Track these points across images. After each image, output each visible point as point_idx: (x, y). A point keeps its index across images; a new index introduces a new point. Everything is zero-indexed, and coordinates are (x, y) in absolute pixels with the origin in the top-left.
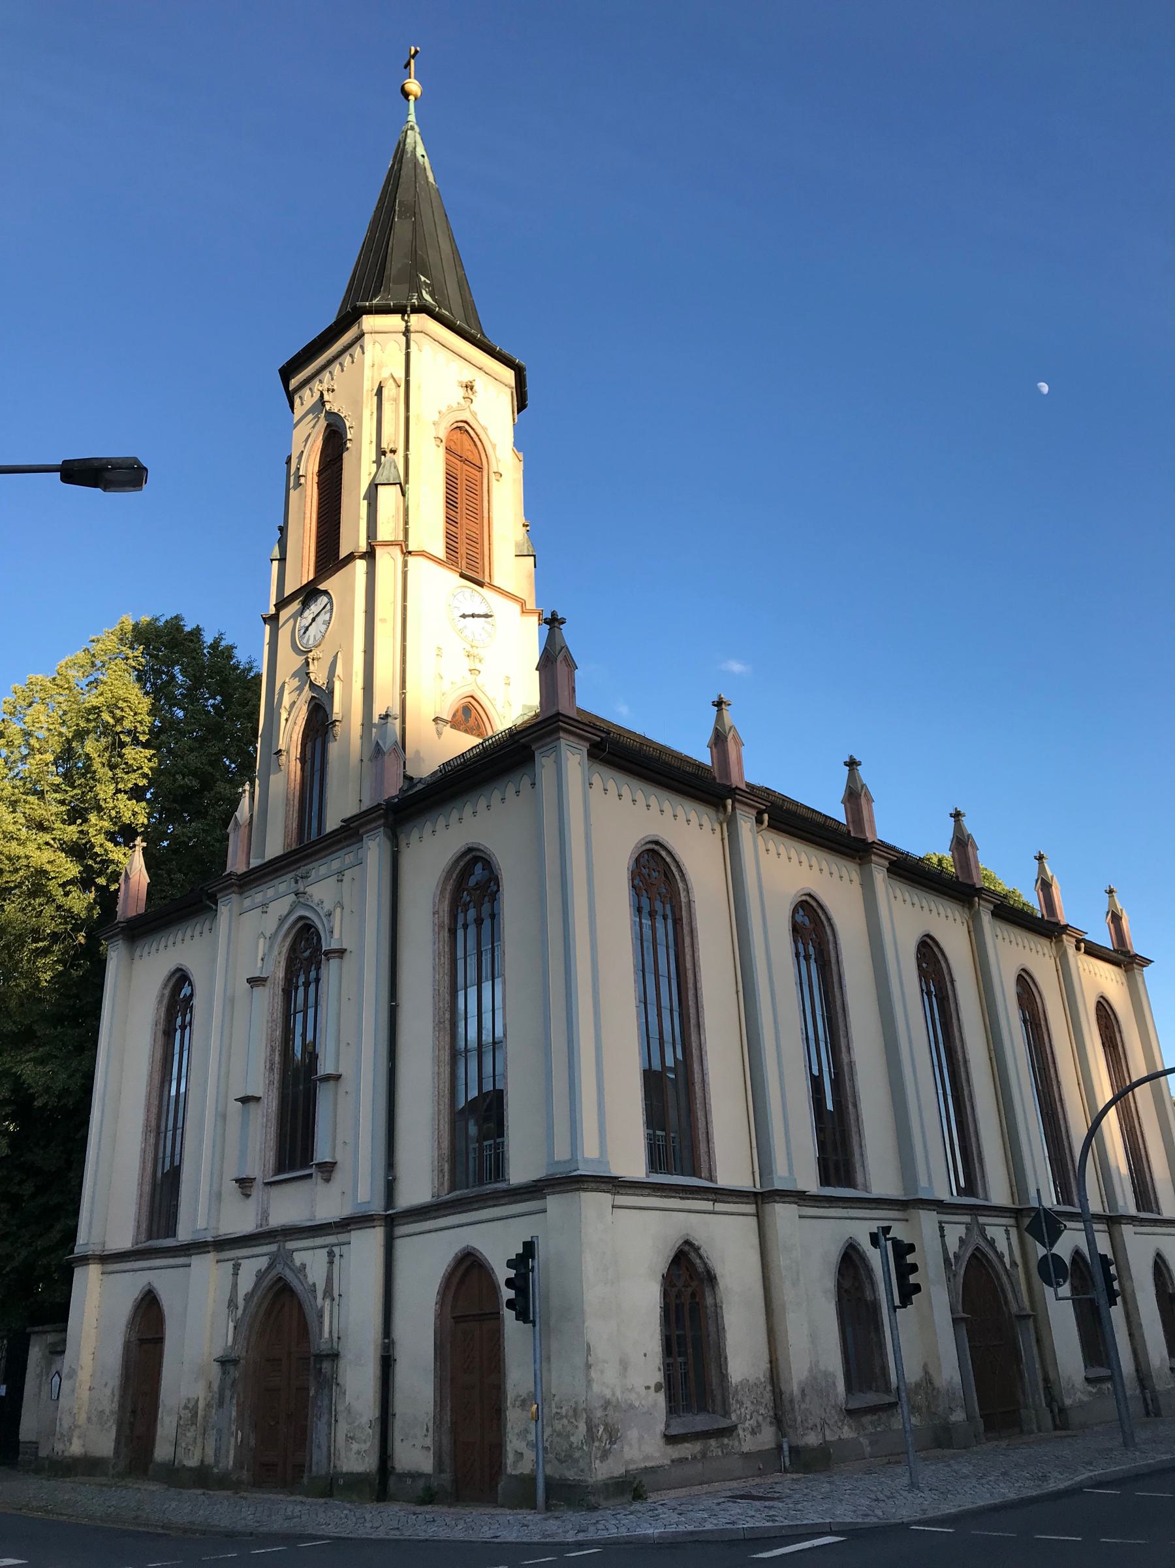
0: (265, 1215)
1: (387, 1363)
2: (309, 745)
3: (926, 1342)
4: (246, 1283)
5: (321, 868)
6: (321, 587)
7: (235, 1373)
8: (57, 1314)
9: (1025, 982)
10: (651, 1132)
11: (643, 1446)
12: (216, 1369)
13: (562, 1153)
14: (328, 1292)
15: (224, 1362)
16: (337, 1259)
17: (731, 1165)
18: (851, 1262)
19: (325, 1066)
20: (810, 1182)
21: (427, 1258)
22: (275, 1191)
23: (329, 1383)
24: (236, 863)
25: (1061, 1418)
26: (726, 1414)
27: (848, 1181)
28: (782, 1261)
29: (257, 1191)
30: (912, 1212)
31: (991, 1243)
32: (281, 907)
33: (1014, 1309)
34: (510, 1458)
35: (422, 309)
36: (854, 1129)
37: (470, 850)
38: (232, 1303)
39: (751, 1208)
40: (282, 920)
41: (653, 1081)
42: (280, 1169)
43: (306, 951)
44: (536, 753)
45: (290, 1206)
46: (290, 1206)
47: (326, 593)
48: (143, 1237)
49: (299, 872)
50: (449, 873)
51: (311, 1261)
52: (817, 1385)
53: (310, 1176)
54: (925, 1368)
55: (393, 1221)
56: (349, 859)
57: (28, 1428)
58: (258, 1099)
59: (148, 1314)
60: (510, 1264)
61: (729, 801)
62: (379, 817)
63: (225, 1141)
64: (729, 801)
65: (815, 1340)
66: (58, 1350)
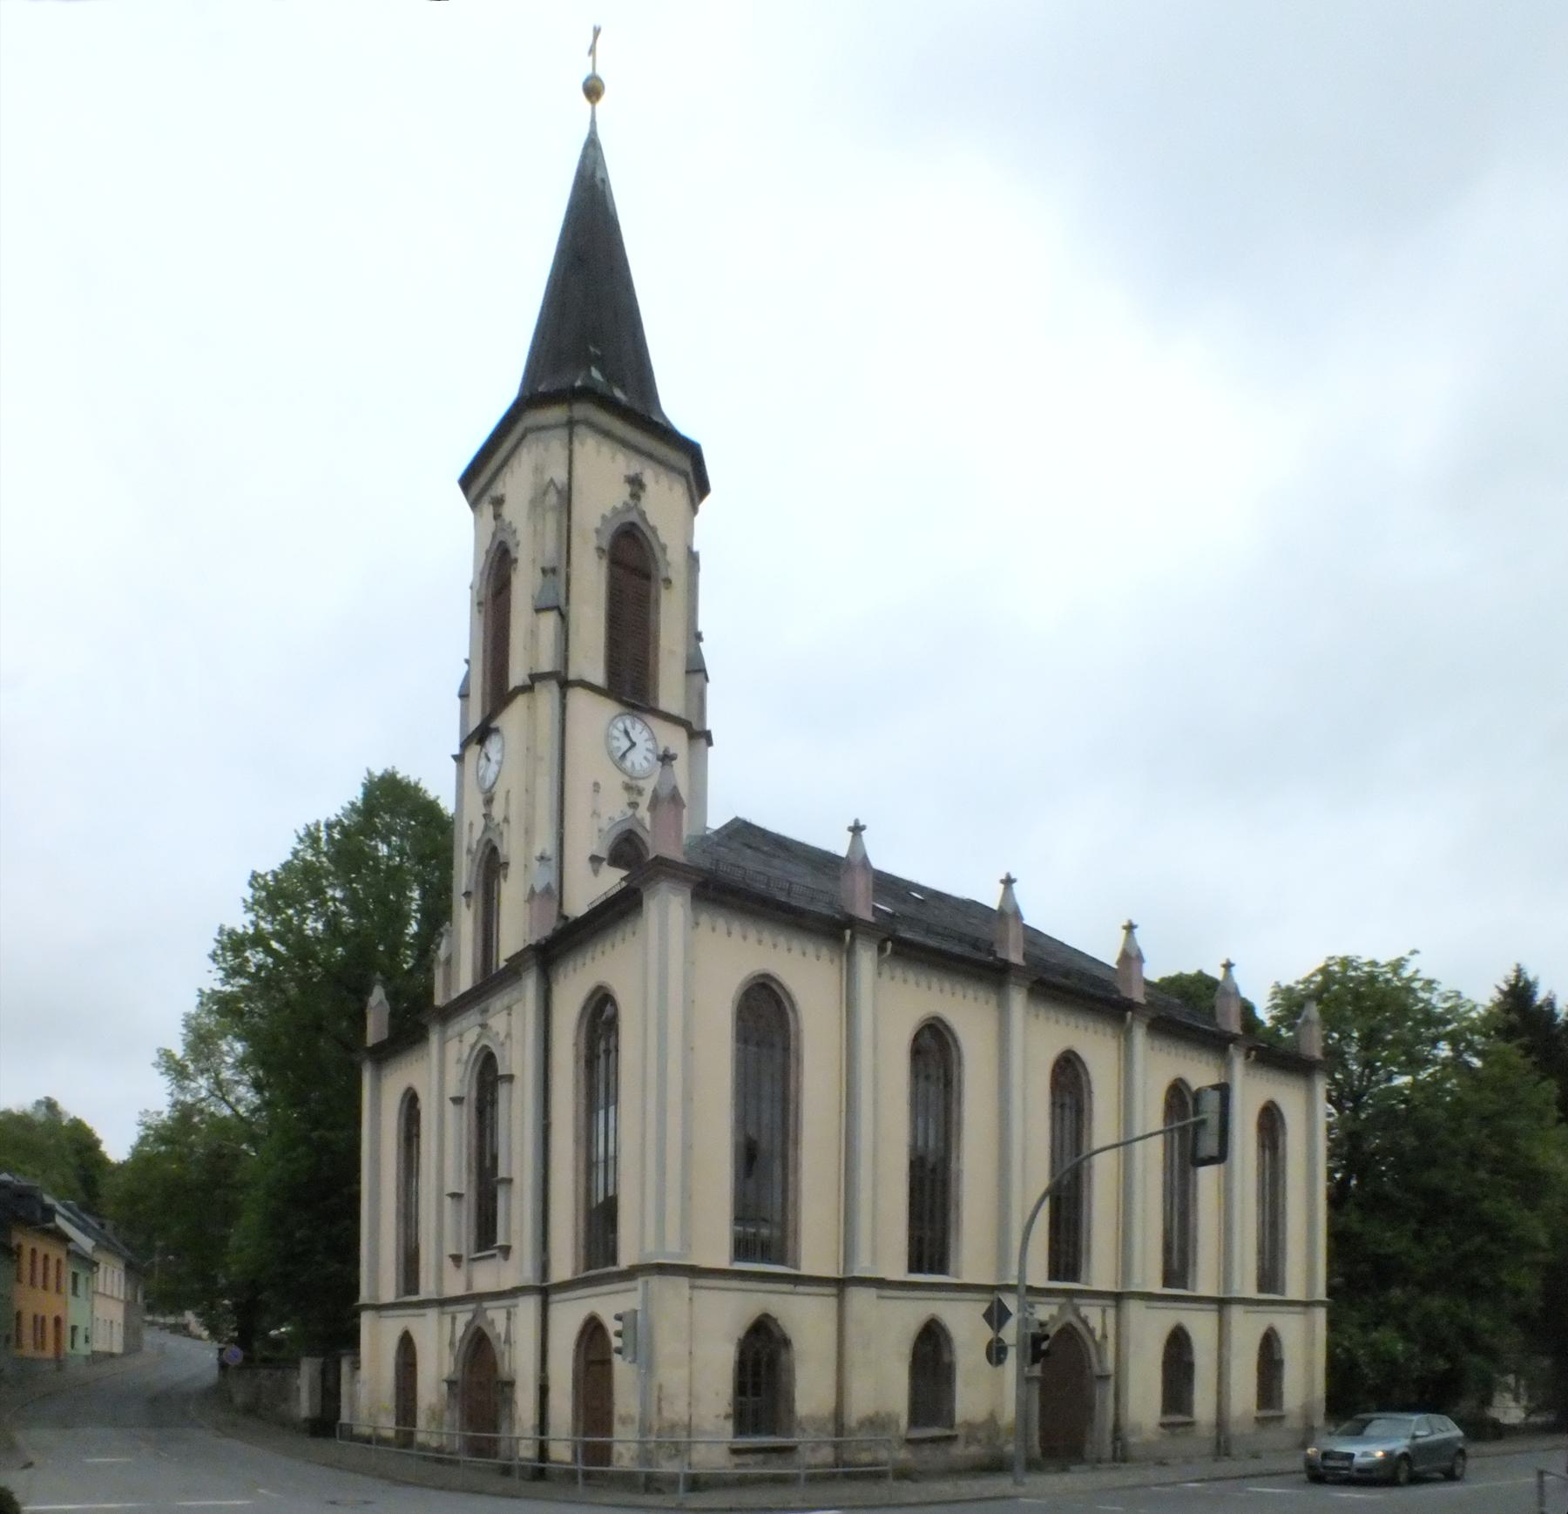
0: (469, 1285)
1: (543, 1391)
3: (987, 1392)
4: (460, 1330)
5: (498, 1002)
6: (493, 725)
8: (351, 1340)
10: (740, 1229)
11: (712, 1456)
12: (445, 1386)
13: (650, 1246)
14: (508, 1341)
17: (816, 1252)
19: (502, 1173)
21: (568, 1318)
23: (509, 1401)
24: (439, 1000)
25: (1121, 1454)
27: (940, 1266)
28: (851, 1329)
31: (1084, 1322)
32: (471, 1036)
33: (1097, 1370)
35: (588, 394)
38: (452, 1344)
39: (833, 1290)
40: (473, 1047)
41: (918, 1166)
43: (488, 1075)
45: (488, 1277)
46: (488, 1277)
48: (581, 1268)
49: (483, 1005)
50: (584, 1008)
51: (496, 1315)
52: (876, 1423)
53: (493, 1256)
55: (545, 1292)
56: (515, 994)
57: (345, 1418)
59: (406, 1344)
61: (848, 933)
63: (446, 1227)
64: (848, 933)
65: (884, 1386)
66: (356, 1366)
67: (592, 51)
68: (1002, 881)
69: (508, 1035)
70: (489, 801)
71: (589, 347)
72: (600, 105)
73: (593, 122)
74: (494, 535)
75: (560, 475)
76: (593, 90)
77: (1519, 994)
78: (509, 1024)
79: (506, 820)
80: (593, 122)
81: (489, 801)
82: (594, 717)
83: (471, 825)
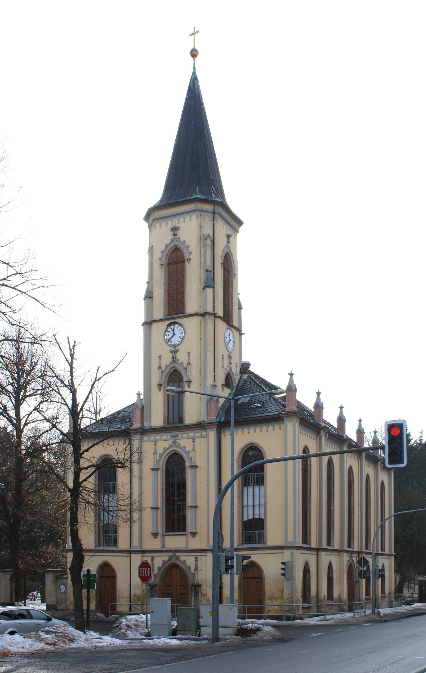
0: (163, 546)
2: (209, 403)
14: (196, 569)
16: (199, 560)
18: (350, 567)
22: (166, 538)
29: (159, 537)
30: (342, 553)
36: (332, 529)
37: (252, 444)
39: (315, 553)
40: (165, 450)
42: (168, 530)
44: (285, 420)
45: (175, 542)
47: (180, 325)
54: (339, 594)
60: (184, 561)
62: (215, 425)
67: (113, 370)
68: (316, 393)
69: (194, 450)
70: (174, 352)
71: (193, 171)
72: (196, 59)
73: (194, 68)
74: (172, 241)
75: (211, 234)
76: (194, 54)
77: (396, 432)
78: (194, 445)
79: (189, 364)
80: (194, 68)
81: (174, 352)
82: (221, 325)
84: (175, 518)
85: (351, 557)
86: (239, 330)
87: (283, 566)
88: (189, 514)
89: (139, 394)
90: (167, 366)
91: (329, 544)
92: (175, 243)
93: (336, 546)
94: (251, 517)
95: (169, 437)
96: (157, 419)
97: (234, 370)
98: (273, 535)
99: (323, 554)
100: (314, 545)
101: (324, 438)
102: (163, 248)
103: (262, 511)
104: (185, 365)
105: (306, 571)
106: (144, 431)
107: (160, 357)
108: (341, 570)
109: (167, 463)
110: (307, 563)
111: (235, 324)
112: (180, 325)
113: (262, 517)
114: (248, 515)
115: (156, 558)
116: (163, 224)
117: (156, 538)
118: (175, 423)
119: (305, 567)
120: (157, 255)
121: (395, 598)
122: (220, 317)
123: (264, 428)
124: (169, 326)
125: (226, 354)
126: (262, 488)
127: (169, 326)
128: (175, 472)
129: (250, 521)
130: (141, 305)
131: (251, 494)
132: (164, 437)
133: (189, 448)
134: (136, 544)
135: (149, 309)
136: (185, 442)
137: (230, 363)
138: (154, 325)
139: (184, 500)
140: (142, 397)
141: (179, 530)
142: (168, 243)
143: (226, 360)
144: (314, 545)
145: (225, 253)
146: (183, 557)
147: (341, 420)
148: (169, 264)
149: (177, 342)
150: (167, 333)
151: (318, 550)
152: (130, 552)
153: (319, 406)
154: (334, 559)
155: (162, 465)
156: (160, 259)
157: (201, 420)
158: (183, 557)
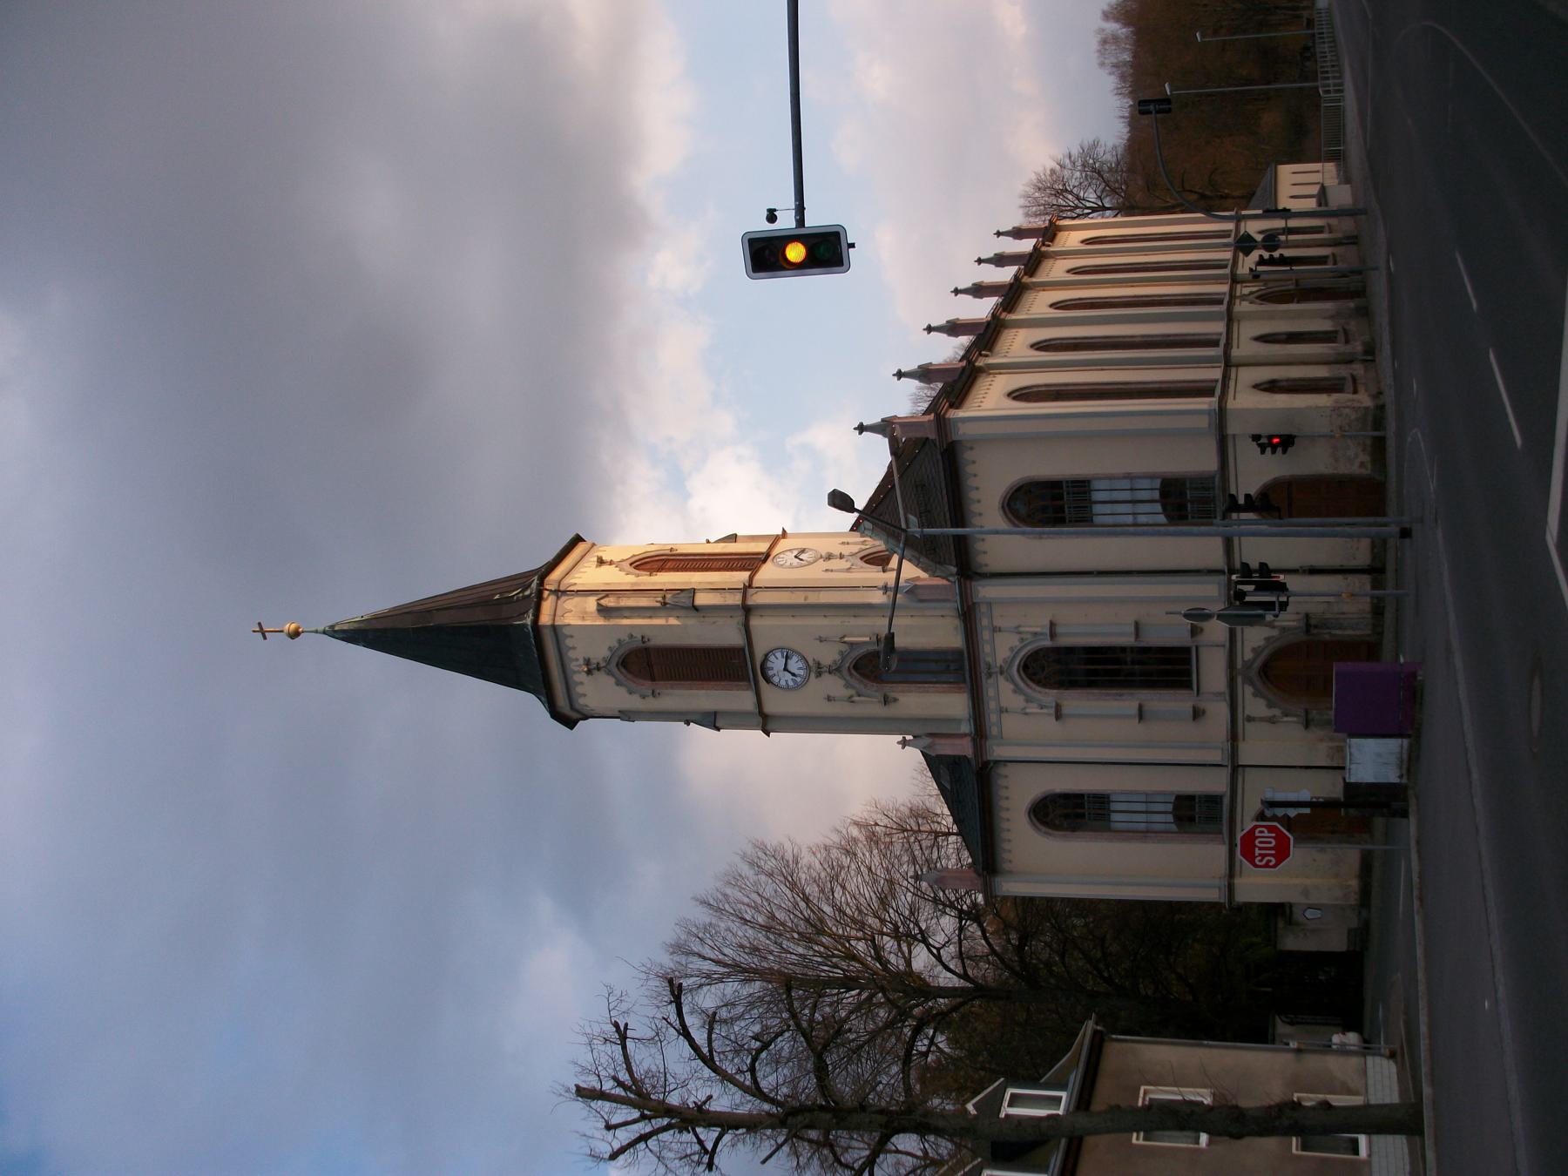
1: (1293, 338)
7: (1314, 714)
9: (1019, 395)
15: (1307, 725)
20: (1215, 400)
26: (1344, 379)
29: (1202, 705)
32: (1005, 687)
34: (1364, 472)
38: (1271, 720)
39: (1233, 370)
40: (1017, 690)
42: (1187, 685)
45: (1212, 671)
47: (766, 656)
58: (1140, 707)
60: (1254, 650)
74: (610, 673)
81: (818, 670)
82: (766, 574)
83: (829, 699)
84: (1159, 668)
85: (1243, 297)
86: (776, 540)
87: (1269, 450)
88: (1153, 639)
89: (904, 743)
90: (848, 685)
91: (1215, 344)
92: (613, 666)
93: (1218, 328)
94: (1158, 507)
95: (991, 681)
96: (952, 704)
97: (855, 549)
98: (1199, 460)
99: (1235, 353)
100: (1216, 374)
101: (990, 361)
102: (622, 691)
103: (1146, 484)
104: (844, 648)
105: (1272, 387)
106: (980, 734)
107: (829, 699)
108: (1271, 316)
109: (1045, 686)
110: (1257, 387)
111: (762, 547)
112: (766, 656)
113: (1157, 483)
114: (1154, 513)
115: (1247, 712)
116: (579, 689)
117: (1204, 712)
118: (961, 667)
119: (1265, 390)
120: (634, 702)
121: (1347, 342)
122: (751, 578)
123: (971, 482)
124: (768, 680)
125: (822, 565)
126: (1096, 485)
127: (768, 680)
128: (1067, 668)
129: (1167, 516)
130: (730, 736)
131: (1108, 508)
132: (991, 692)
133: (1014, 641)
134: (1216, 756)
135: (737, 720)
136: (1001, 648)
137: (841, 556)
138: (769, 708)
139: (1123, 649)
140: (909, 737)
141: (1188, 661)
142: (613, 680)
143: (835, 564)
144: (1216, 374)
145: (631, 569)
146: (1246, 654)
147: (953, 328)
148: (653, 679)
149: (800, 664)
150: (783, 683)
151: (1229, 364)
152: (1236, 769)
153: (925, 374)
154: (1246, 332)
155: (1050, 696)
156: (644, 697)
157: (954, 613)
158: (1246, 654)
